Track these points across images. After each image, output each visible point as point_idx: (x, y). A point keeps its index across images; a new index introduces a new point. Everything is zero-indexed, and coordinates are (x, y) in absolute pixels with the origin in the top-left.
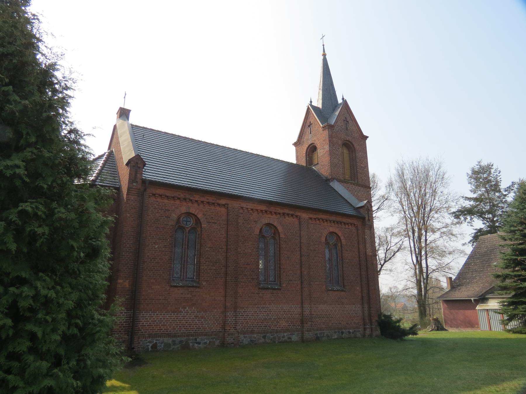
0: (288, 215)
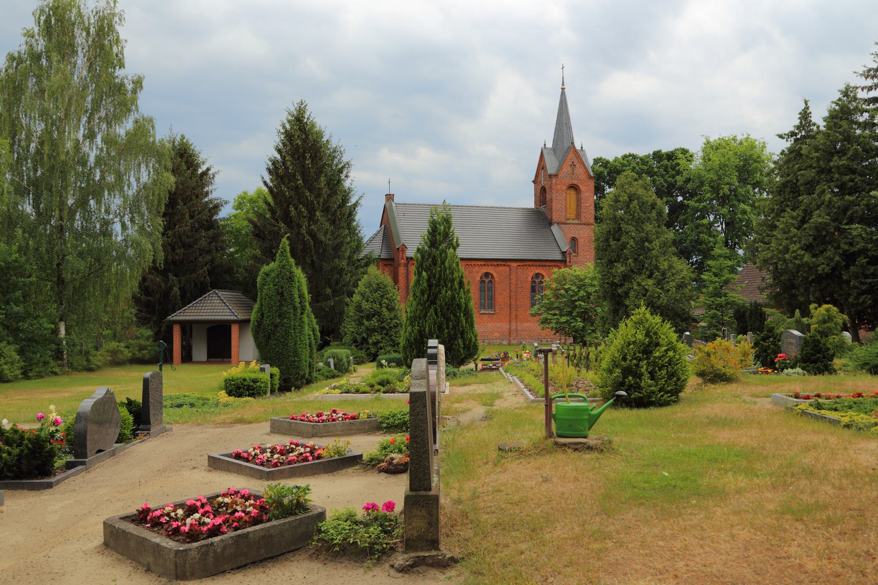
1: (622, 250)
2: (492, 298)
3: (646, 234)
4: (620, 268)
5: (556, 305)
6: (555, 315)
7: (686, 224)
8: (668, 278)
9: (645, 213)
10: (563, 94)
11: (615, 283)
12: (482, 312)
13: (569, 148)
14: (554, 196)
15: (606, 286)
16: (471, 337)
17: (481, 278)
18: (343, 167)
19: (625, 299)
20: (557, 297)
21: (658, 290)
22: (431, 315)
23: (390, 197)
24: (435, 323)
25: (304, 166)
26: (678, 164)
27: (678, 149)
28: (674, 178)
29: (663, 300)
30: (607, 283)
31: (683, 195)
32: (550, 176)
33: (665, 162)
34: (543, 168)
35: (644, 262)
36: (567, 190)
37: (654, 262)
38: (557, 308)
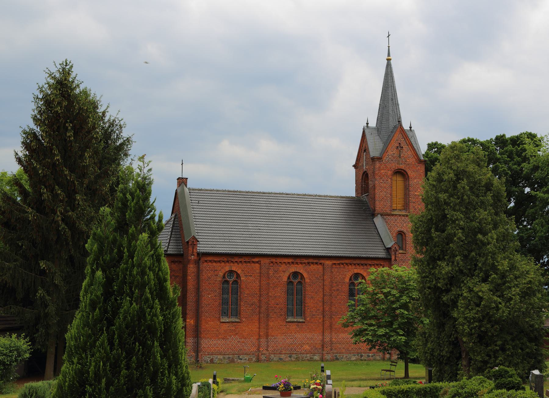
0: (313, 263)
1: (448, 244)
2: (301, 303)
3: (479, 223)
4: (445, 268)
5: (373, 313)
6: (371, 325)
7: (534, 219)
8: (509, 282)
9: (477, 196)
10: (389, 66)
11: (439, 288)
12: (289, 320)
13: (395, 127)
14: (377, 182)
15: (427, 291)
16: (170, 383)
17: (289, 278)
18: (122, 144)
19: (453, 310)
20: (375, 302)
21: (495, 298)
22: (102, 344)
23: (182, 181)
24: (108, 359)
25: (66, 140)
26: (525, 150)
27: (523, 133)
28: (519, 165)
29: (503, 312)
30: (429, 288)
31: (531, 186)
32: (373, 159)
33: (510, 147)
34: (365, 151)
35: (477, 261)
36: (392, 175)
37: (490, 261)
38: (375, 317)
